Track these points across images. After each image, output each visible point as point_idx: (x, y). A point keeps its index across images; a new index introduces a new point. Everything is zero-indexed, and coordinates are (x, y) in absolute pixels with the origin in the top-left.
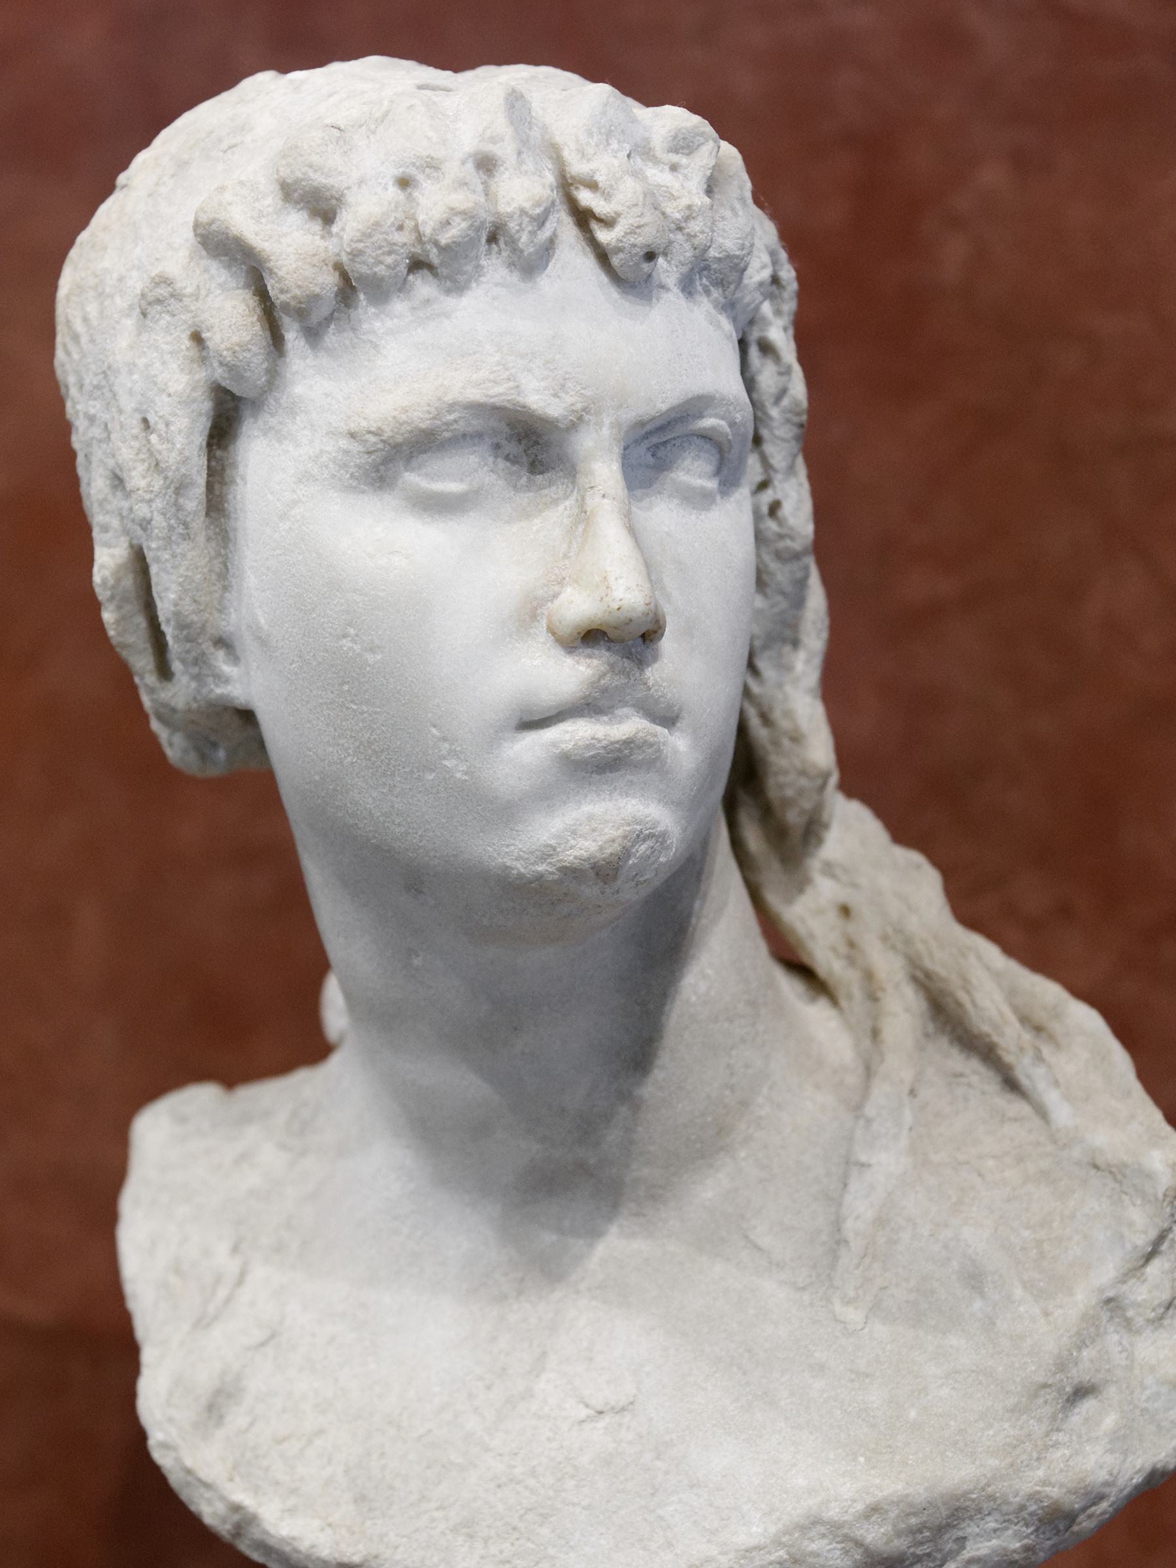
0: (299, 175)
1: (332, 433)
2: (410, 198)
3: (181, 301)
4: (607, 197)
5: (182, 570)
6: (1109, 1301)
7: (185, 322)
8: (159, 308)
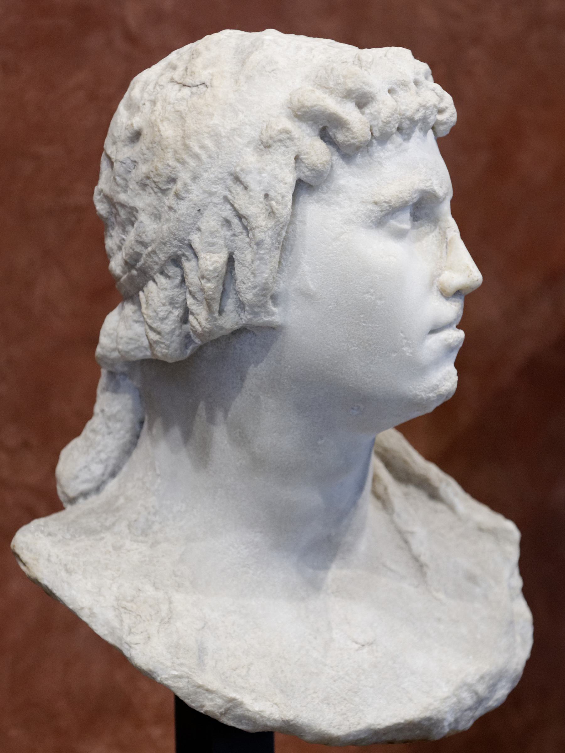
0: (359, 87)
1: (363, 202)
3: (292, 141)
5: (273, 264)
7: (294, 150)
8: (279, 144)
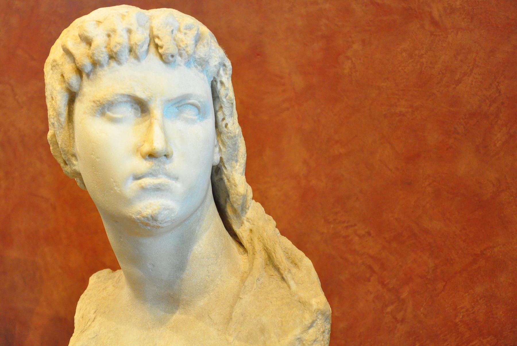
2: (110, 40)
4: (161, 41)
6: (299, 339)
